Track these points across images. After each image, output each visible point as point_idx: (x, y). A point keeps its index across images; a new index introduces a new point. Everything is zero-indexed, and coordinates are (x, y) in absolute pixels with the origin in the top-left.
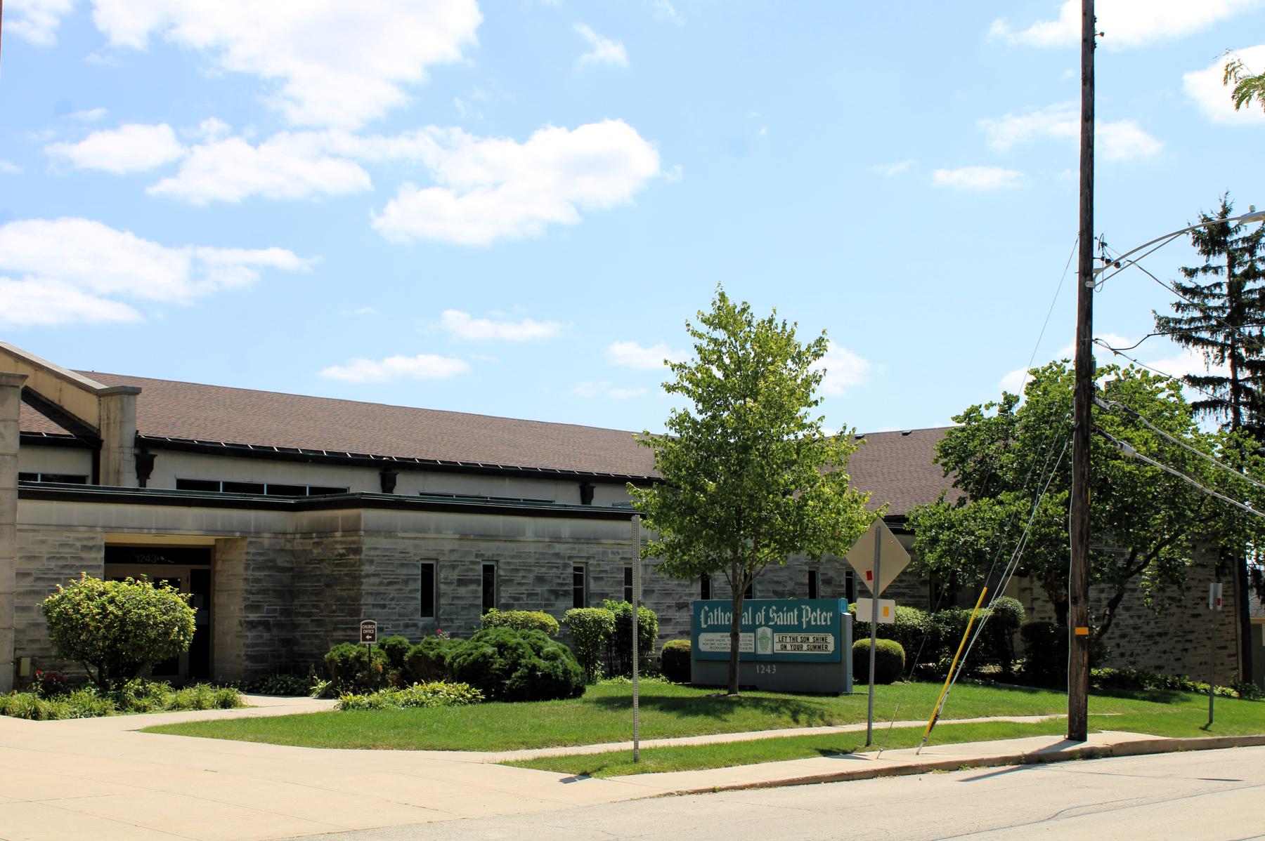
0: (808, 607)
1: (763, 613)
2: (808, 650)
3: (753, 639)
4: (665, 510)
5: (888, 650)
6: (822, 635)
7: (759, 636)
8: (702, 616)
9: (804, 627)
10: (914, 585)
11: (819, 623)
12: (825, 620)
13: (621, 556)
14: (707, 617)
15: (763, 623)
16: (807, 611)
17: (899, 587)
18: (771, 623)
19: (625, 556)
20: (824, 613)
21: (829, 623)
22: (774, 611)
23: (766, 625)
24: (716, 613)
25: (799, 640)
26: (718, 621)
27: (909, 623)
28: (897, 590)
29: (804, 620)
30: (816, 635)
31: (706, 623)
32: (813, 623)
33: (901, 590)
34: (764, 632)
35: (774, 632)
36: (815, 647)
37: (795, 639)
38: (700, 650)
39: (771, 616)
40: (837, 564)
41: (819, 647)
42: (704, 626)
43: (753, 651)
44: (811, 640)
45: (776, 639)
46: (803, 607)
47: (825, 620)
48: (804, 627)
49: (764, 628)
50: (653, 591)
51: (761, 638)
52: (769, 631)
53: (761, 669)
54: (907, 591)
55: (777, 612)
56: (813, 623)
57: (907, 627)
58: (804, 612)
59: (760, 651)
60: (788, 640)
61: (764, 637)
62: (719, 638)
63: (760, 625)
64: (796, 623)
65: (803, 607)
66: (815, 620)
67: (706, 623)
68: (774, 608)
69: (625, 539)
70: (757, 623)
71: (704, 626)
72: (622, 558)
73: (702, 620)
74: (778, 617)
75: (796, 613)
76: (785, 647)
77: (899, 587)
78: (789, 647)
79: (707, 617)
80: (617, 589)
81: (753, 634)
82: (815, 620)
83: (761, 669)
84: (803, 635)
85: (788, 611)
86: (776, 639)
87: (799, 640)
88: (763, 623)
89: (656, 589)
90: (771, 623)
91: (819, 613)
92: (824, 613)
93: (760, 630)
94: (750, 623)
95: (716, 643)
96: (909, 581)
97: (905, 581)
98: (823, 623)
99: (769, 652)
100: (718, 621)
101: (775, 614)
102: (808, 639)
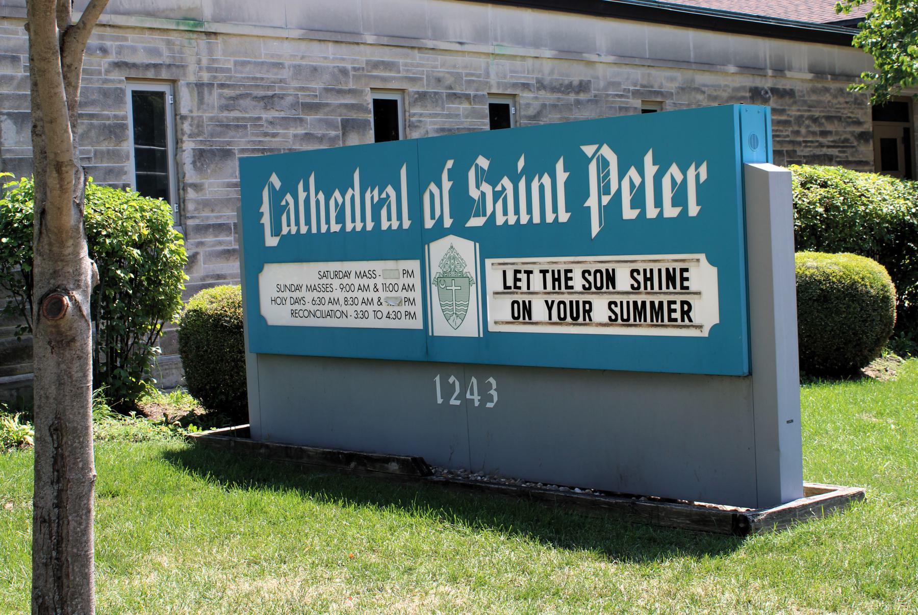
0: (607, 152)
1: (447, 185)
2: (612, 321)
3: (416, 281)
4: (859, 342)
5: (854, 283)
6: (668, 261)
7: (435, 270)
8: (265, 208)
9: (595, 229)
10: (846, 140)
11: (652, 212)
12: (680, 198)
13: (113, 58)
14: (278, 211)
15: (448, 222)
16: (604, 164)
17: (821, 145)
18: (476, 222)
19: (130, 59)
20: (674, 170)
21: (694, 210)
22: (482, 176)
23: (460, 230)
24: (302, 195)
25: (578, 282)
26: (308, 222)
27: (886, 209)
28: (818, 152)
29: (592, 202)
30: (643, 261)
31: (276, 231)
32: (629, 214)
33: (825, 150)
34: (452, 256)
35: (485, 254)
36: (639, 310)
37: (561, 280)
38: (263, 319)
39: (474, 193)
40: (700, 97)
41: (657, 311)
42: (272, 241)
43: (418, 324)
44: (623, 281)
45: (494, 282)
46: (589, 150)
47: (680, 198)
48: (595, 229)
49: (451, 239)
50: (226, 154)
51: (444, 276)
52: (466, 249)
53: (448, 391)
54: (831, 151)
55: (492, 177)
56: (629, 214)
57: (883, 219)
58: (593, 168)
59: (441, 328)
60: (537, 279)
61: (452, 274)
62: (314, 280)
63: (439, 232)
64: (564, 217)
65: (589, 150)
66: (638, 201)
67: (276, 231)
68: (483, 162)
69: (128, 13)
70: (429, 224)
71: (272, 241)
72: (118, 65)
73: (266, 220)
74: (496, 196)
75: (562, 176)
76: (527, 309)
77: (821, 145)
78: (539, 311)
79: (278, 211)
80: (104, 147)
81: (414, 265)
82: (638, 201)
83: (448, 391)
84: (592, 262)
85: (530, 174)
86: (494, 282)
87: (578, 282)
88: (448, 222)
89: (236, 148)
90: (476, 222)
91: (650, 169)
92: (674, 170)
93: (438, 250)
94: (406, 224)
95: (309, 296)
96: (837, 133)
97: (830, 133)
98: (671, 212)
99: (469, 328)
100: (308, 222)
101: (487, 188)
102: (611, 278)
